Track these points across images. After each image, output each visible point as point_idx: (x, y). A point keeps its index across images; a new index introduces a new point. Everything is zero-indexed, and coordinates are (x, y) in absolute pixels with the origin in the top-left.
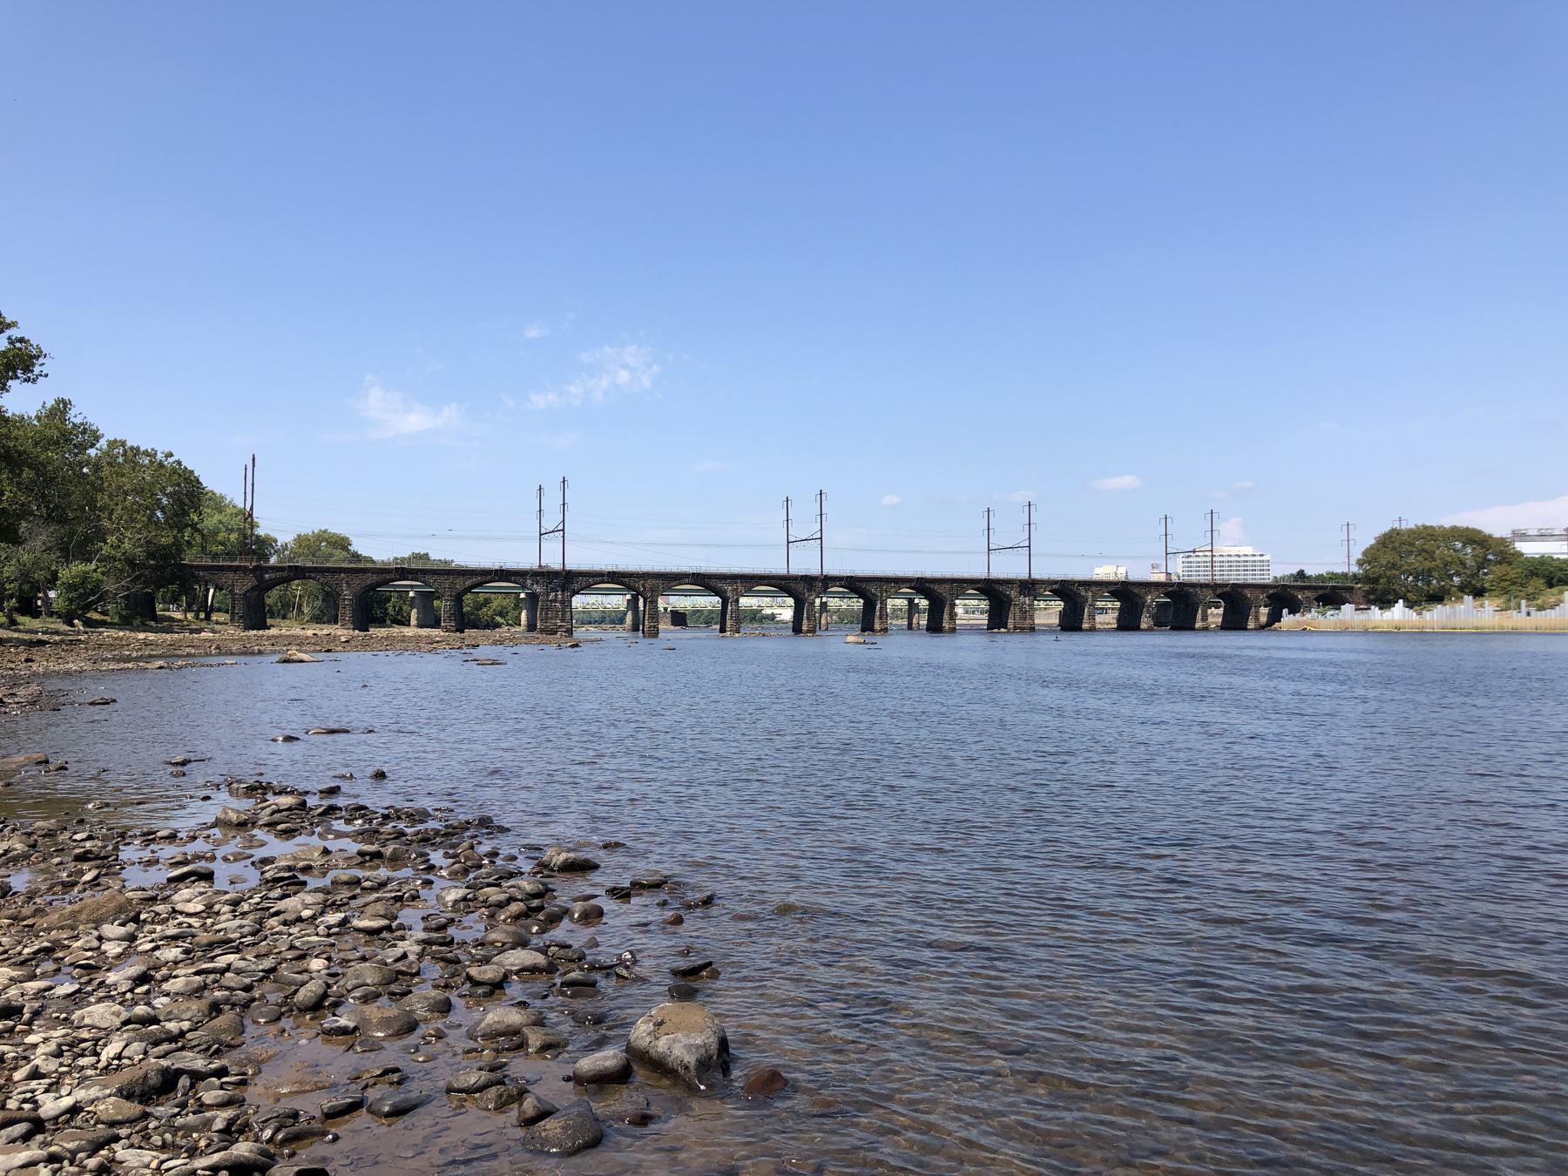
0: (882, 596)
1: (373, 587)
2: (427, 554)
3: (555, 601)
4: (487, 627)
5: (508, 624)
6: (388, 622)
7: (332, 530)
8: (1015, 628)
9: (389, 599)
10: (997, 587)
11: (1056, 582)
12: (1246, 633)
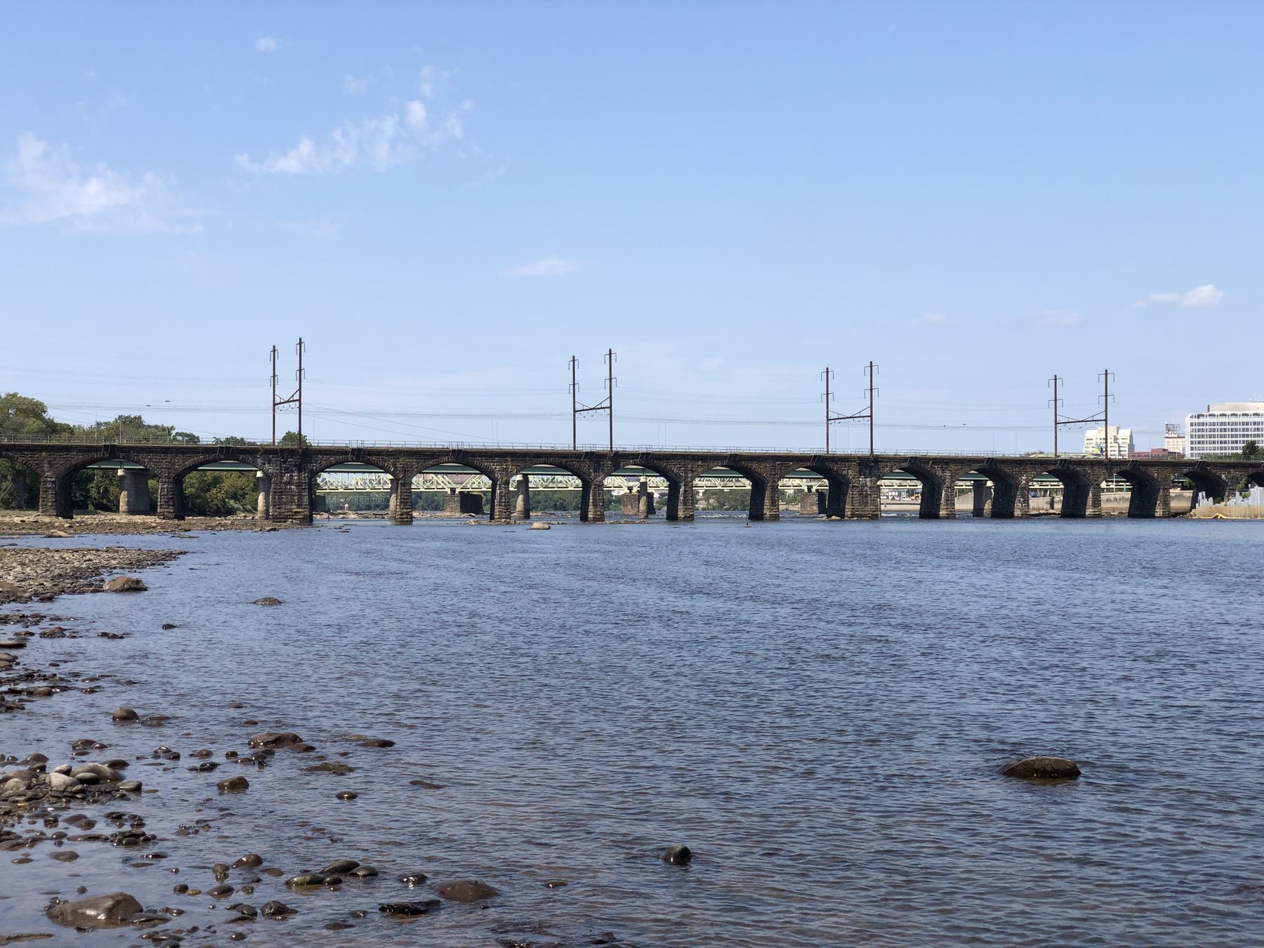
0: (686, 477)
1: (83, 465)
2: (140, 418)
3: (290, 483)
4: (218, 512)
5: (245, 510)
6: (91, 507)
7: (23, 393)
8: (853, 515)
9: (91, 479)
10: (830, 465)
11: (904, 459)
12: (938, 521)
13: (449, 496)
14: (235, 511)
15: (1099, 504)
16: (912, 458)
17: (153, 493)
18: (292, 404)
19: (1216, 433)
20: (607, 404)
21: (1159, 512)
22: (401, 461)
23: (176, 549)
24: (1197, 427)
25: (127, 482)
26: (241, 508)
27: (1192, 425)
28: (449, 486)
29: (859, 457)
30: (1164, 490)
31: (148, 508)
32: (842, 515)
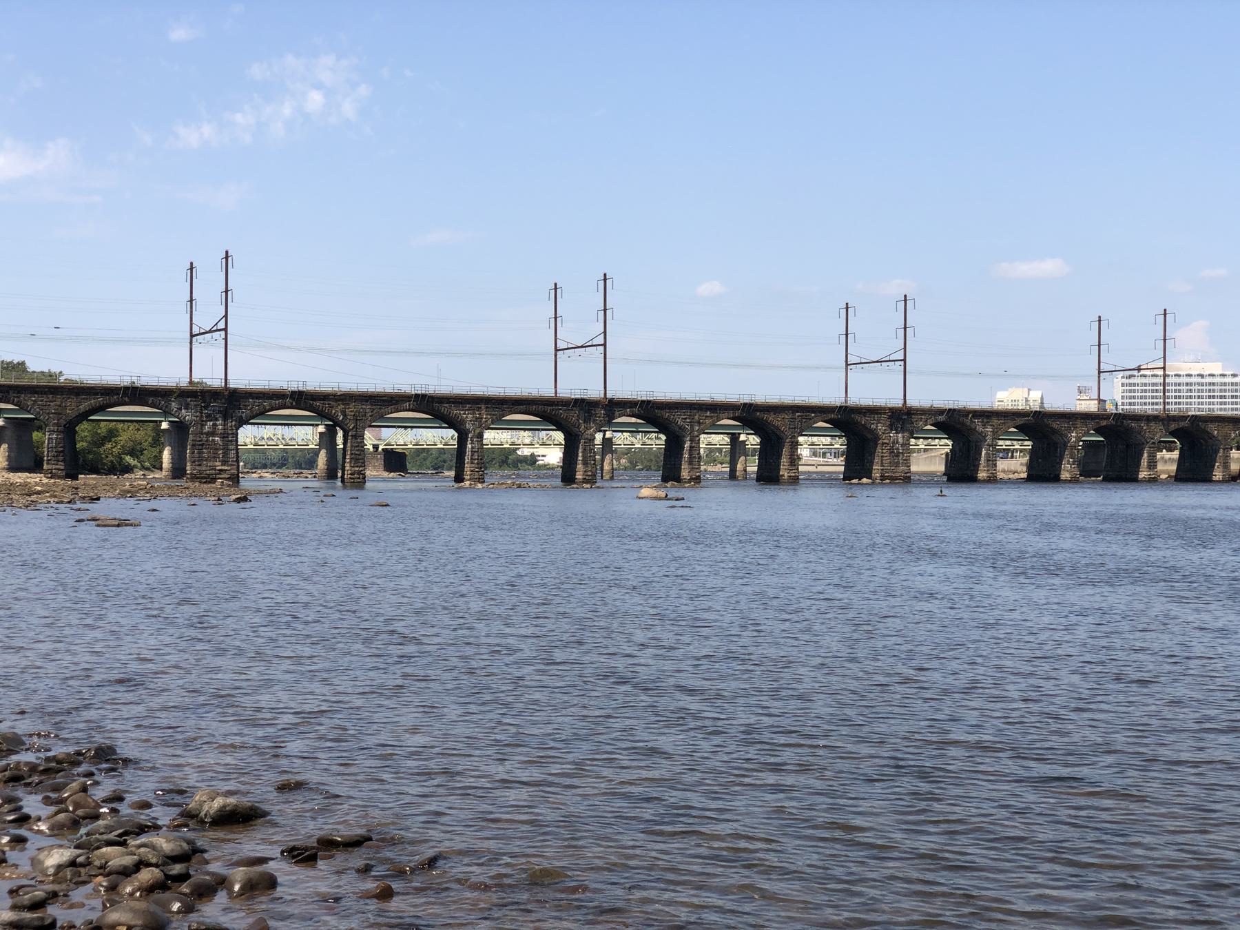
0: (692, 430)
2: (23, 363)
3: (213, 433)
5: (143, 468)
8: (883, 478)
11: (941, 412)
12: (976, 485)
13: (371, 453)
14: (132, 469)
15: (1155, 466)
16: (950, 410)
17: (38, 448)
18: (216, 335)
19: (1148, 394)
20: (600, 340)
21: (1218, 475)
22: (352, 409)
23: (87, 528)
24: (1128, 388)
25: (8, 433)
26: (139, 465)
27: (1123, 385)
28: (371, 442)
29: (890, 409)
30: (1224, 449)
31: (32, 464)
32: (678, 479)
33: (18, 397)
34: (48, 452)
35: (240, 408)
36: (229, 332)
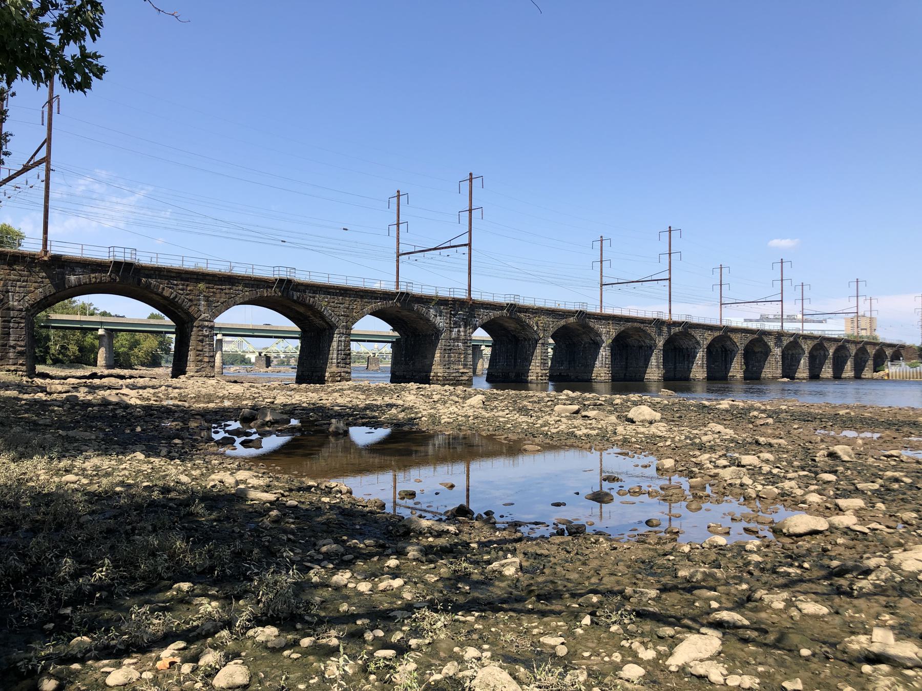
3: (457, 339)
6: (49, 361)
12: (864, 382)
33: (314, 297)
34: (338, 354)
35: (475, 317)
36: (472, 247)
